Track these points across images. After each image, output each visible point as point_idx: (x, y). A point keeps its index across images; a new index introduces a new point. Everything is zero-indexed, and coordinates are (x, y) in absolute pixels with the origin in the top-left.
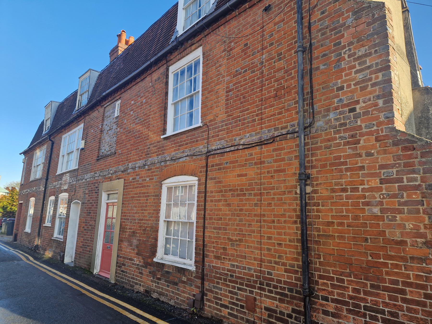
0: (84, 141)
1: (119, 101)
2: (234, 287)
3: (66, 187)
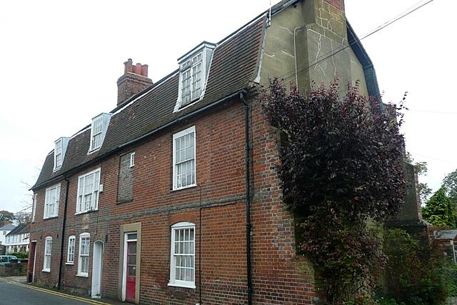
0: (102, 185)
1: (134, 153)
2: (226, 296)
3: (86, 227)
